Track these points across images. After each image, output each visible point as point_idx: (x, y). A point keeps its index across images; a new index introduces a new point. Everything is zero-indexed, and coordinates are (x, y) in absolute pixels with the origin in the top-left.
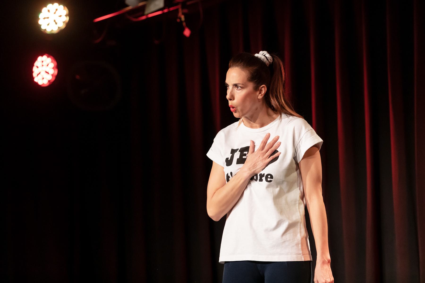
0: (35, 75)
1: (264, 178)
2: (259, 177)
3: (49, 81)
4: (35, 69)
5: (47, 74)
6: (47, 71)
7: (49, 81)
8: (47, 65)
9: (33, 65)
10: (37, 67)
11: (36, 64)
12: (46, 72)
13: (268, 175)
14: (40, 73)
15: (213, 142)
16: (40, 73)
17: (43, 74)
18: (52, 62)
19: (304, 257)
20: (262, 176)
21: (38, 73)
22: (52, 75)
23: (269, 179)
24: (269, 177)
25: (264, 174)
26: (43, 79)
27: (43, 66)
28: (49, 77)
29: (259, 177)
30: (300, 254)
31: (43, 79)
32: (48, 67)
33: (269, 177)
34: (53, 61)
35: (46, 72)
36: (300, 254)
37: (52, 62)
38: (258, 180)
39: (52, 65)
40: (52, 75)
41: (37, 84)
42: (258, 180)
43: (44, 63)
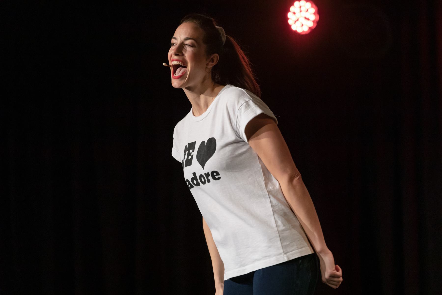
0: (290, 22)
1: (210, 178)
2: (199, 181)
3: (310, 28)
4: (290, 15)
5: (306, 20)
6: (307, 17)
7: (310, 28)
8: (307, 11)
9: (289, 11)
10: (294, 13)
11: (292, 9)
12: (306, 18)
13: (212, 173)
14: (298, 20)
15: (271, 110)
16: (298, 20)
17: (302, 20)
18: (312, 7)
19: (287, 256)
20: (207, 175)
21: (296, 19)
22: (313, 21)
23: (217, 177)
24: (215, 174)
25: (208, 173)
26: (302, 25)
27: (301, 11)
28: (311, 24)
29: (199, 181)
30: (281, 254)
31: (302, 25)
33: (215, 175)
34: (314, 6)
35: (306, 18)
36: (281, 254)
37: (312, 7)
38: (207, 182)
39: (313, 10)
40: (313, 21)
41: (295, 32)
42: (207, 182)
43: (302, 9)
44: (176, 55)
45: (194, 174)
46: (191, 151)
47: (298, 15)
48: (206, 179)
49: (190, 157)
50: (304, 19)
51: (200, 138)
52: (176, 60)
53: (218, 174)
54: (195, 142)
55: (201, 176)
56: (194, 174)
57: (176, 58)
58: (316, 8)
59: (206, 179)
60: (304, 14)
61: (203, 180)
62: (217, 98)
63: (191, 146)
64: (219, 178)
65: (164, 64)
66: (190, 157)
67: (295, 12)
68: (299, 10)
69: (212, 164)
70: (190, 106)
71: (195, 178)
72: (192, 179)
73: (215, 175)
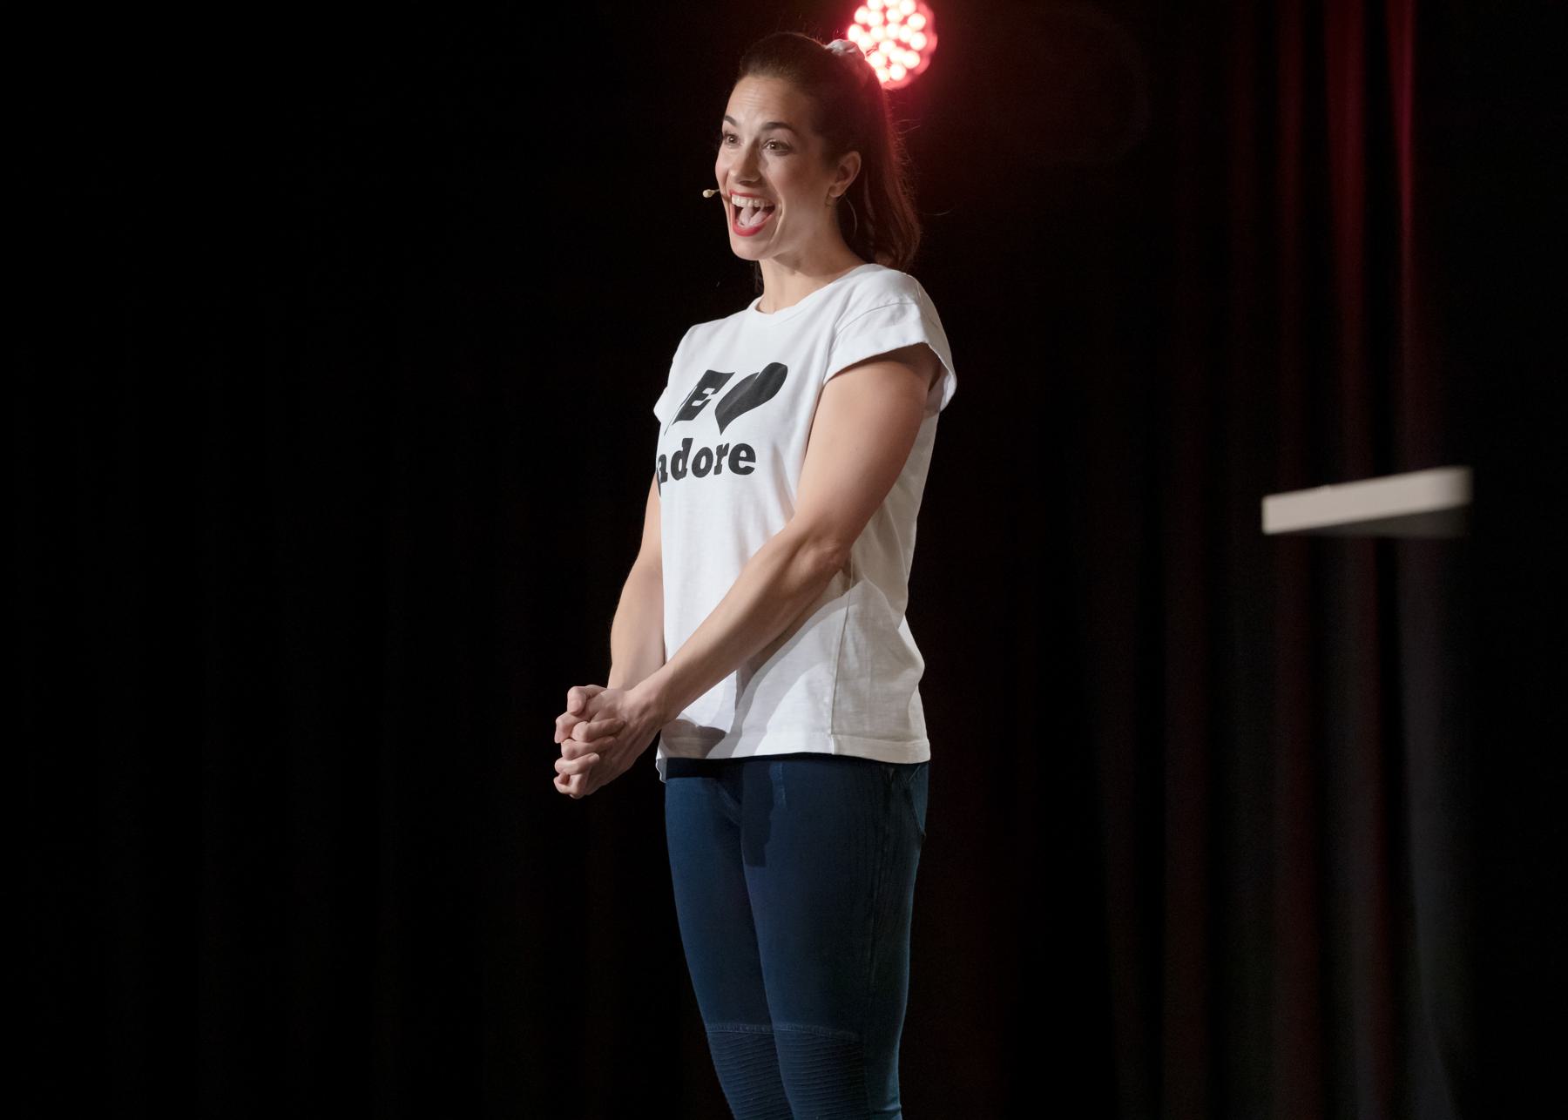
1: (725, 460)
3: (910, 71)
6: (904, 39)
7: (910, 71)
17: (888, 48)
19: (838, 743)
22: (920, 53)
23: (742, 464)
24: (743, 454)
27: (886, 22)
32: (905, 27)
33: (740, 458)
34: (924, 7)
40: (920, 53)
43: (889, 15)
44: (747, 184)
45: (687, 443)
46: (708, 391)
47: (877, 33)
48: (715, 464)
49: (697, 403)
50: (893, 45)
51: (744, 366)
52: (743, 195)
53: (751, 456)
54: (730, 375)
55: (706, 452)
56: (687, 443)
57: (741, 189)
58: (930, 15)
59: (715, 464)
60: (894, 31)
61: (704, 460)
62: (832, 286)
63: (713, 379)
64: (748, 470)
65: (706, 194)
66: (697, 403)
67: (871, 23)
68: (880, 18)
69: (743, 429)
70: (760, 292)
71: (680, 456)
72: (677, 456)
73: (740, 458)
